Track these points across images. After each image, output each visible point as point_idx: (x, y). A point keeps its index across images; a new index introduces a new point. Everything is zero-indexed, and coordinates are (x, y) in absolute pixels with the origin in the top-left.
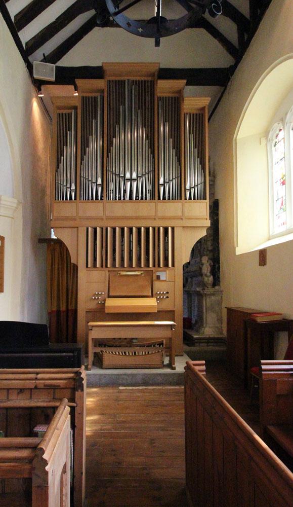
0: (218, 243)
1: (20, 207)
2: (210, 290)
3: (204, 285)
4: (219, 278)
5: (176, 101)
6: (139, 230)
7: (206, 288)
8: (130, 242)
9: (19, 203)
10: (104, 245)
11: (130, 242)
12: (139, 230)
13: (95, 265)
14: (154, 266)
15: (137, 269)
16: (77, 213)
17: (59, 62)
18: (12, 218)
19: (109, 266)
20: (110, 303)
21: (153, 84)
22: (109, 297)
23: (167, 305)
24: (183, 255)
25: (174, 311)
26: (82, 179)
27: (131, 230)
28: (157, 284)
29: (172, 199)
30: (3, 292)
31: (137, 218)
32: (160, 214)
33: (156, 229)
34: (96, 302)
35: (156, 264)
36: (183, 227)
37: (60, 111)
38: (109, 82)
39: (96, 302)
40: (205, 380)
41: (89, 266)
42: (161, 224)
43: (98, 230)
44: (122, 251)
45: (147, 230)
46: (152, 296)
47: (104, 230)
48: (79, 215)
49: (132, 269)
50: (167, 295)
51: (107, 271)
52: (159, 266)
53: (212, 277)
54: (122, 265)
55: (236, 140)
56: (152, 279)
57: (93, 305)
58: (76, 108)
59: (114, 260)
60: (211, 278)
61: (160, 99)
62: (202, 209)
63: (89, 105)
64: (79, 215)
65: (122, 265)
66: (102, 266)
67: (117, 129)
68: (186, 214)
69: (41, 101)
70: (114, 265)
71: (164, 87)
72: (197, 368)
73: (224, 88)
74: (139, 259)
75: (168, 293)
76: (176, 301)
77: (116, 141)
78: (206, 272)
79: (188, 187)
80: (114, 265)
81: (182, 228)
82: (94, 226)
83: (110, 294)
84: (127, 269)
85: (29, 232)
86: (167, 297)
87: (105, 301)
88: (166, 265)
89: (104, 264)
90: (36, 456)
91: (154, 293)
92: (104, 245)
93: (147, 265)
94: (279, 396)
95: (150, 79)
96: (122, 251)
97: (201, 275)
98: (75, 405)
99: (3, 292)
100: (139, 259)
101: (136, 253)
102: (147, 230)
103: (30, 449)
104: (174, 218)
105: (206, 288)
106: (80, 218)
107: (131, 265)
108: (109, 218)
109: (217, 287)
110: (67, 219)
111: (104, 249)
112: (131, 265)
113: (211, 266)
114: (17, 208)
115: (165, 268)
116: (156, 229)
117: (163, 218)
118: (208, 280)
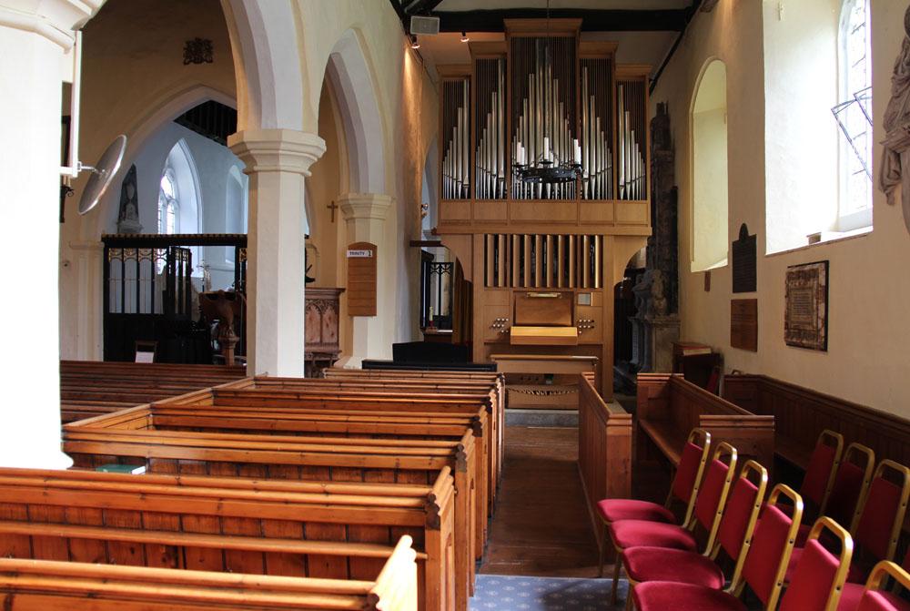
0: (676, 251)
1: (395, 203)
2: (661, 319)
3: (654, 311)
4: (676, 301)
5: (604, 67)
6: (555, 238)
7: (657, 316)
8: (543, 253)
9: (393, 199)
10: (508, 258)
11: (543, 253)
12: (555, 238)
13: (496, 284)
14: (575, 286)
15: (552, 289)
16: (472, 216)
17: (439, 5)
18: (384, 220)
19: (514, 285)
20: (516, 331)
21: (573, 42)
22: (515, 325)
23: (590, 338)
24: (617, 275)
25: (602, 345)
26: (478, 170)
27: (544, 238)
28: (579, 310)
29: (601, 198)
30: (375, 315)
31: (554, 223)
32: (583, 218)
33: (579, 237)
34: (497, 331)
35: (578, 282)
36: (616, 236)
37: (447, 80)
38: (513, 39)
39: (497, 331)
40: (593, 389)
41: (488, 285)
42: (585, 232)
43: (501, 238)
44: (533, 265)
45: (566, 238)
46: (572, 326)
47: (508, 239)
48: (475, 218)
49: (545, 290)
50: (593, 324)
51: (512, 292)
52: (582, 286)
53: (665, 300)
54: (533, 284)
55: (692, 114)
56: (570, 299)
57: (493, 336)
58: (469, 77)
59: (522, 276)
60: (663, 302)
61: (584, 63)
62: (638, 215)
63: (485, 69)
64: (475, 218)
65: (533, 284)
66: (505, 285)
67: (525, 105)
68: (619, 218)
69: (417, 56)
70: (522, 284)
71: (591, 45)
72: (587, 377)
73: (679, 33)
74: (555, 276)
75: (593, 321)
76: (604, 334)
77: (523, 120)
78: (656, 292)
79: (622, 183)
80: (522, 284)
81: (613, 237)
82: (495, 233)
83: (517, 322)
84: (539, 290)
85: (403, 234)
86: (593, 327)
87: (509, 330)
88: (592, 284)
89: (508, 282)
90: (368, 605)
91: (575, 323)
92: (508, 258)
93: (566, 284)
94: (650, 399)
95: (569, 35)
96: (533, 265)
97: (651, 296)
98: (425, 556)
99: (375, 315)
100: (555, 276)
101: (551, 270)
102: (566, 238)
103: (356, 597)
104: (603, 224)
105: (657, 316)
106: (476, 222)
107: (544, 283)
108: (515, 223)
109: (672, 315)
110: (456, 223)
111: (508, 263)
112: (544, 283)
113: (664, 285)
114: (390, 206)
115: (588, 290)
116: (579, 237)
117: (587, 224)
118: (660, 305)
